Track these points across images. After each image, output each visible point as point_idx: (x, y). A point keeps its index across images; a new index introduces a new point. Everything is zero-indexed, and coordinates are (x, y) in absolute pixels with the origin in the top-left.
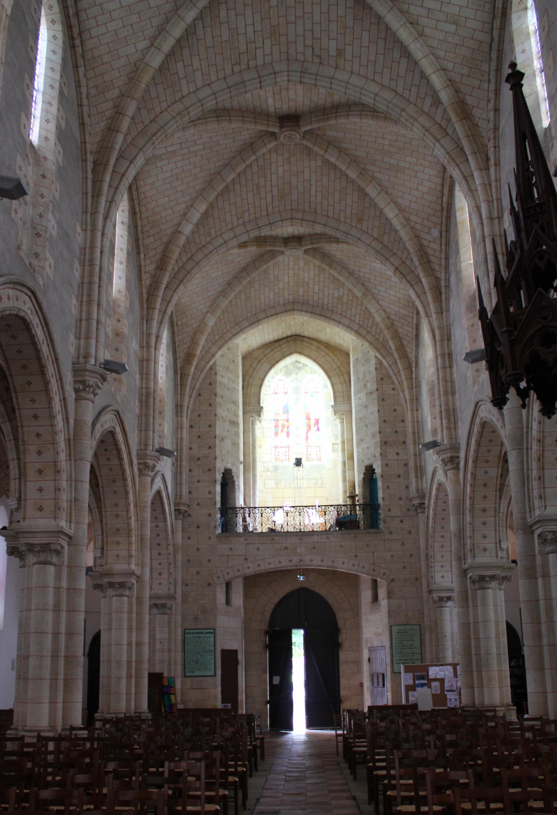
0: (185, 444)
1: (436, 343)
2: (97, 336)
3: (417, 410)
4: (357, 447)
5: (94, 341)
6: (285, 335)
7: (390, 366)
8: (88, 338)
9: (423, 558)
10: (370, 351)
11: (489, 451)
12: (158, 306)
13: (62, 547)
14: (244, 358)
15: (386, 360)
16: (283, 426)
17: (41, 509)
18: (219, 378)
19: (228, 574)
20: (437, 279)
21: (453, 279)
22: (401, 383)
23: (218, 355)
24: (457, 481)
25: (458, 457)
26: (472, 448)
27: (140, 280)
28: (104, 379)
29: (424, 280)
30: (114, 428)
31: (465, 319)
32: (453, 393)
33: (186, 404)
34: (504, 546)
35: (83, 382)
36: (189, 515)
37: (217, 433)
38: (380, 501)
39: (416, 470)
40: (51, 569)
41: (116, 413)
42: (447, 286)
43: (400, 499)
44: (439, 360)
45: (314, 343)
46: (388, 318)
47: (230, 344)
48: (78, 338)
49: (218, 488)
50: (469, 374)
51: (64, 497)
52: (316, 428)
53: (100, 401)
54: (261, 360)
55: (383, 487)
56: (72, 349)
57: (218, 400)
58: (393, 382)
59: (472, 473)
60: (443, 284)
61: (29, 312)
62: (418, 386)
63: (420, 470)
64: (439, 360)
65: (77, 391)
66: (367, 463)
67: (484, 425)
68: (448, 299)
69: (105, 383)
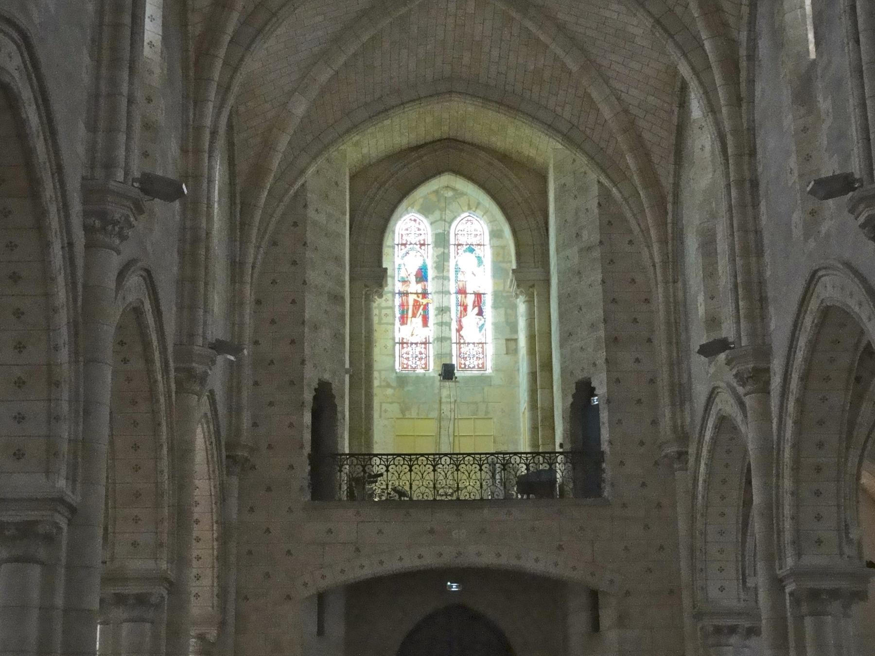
0: (248, 333)
1: (727, 160)
2: (129, 127)
3: (675, 282)
4: (562, 346)
5: (122, 138)
6: (429, 138)
7: (625, 199)
8: (111, 130)
9: (683, 553)
10: (589, 172)
11: (832, 360)
12: (216, 76)
13: (60, 529)
14: (352, 178)
15: (618, 189)
16: (417, 305)
17: (19, 455)
18: (311, 213)
19: (323, 577)
20: (733, 43)
21: (764, 46)
22: (645, 232)
23: (311, 170)
24: (765, 415)
25: (767, 370)
26: (800, 355)
27: (184, 24)
28: (139, 209)
29: (707, 45)
30: (143, 303)
31: (790, 116)
32: (760, 253)
33: (250, 260)
34: (854, 535)
35: (103, 215)
36: (253, 467)
37: (307, 316)
38: (605, 447)
39: (672, 391)
40: (35, 572)
41: (144, 274)
42: (752, 57)
43: (642, 443)
44: (734, 193)
45: (482, 154)
46: (626, 111)
47: (333, 153)
48: (92, 128)
49: (307, 418)
50: (796, 217)
51: (65, 431)
52: (476, 310)
53: (129, 250)
54: (385, 182)
55: (610, 422)
56: (81, 149)
57: (309, 254)
58: (631, 231)
59: (798, 400)
60: (743, 52)
61: (16, 75)
62: (679, 237)
63: (680, 394)
64: (734, 193)
65: (88, 229)
66: (580, 376)
67: (826, 312)
68: (751, 82)
69: (142, 218)
